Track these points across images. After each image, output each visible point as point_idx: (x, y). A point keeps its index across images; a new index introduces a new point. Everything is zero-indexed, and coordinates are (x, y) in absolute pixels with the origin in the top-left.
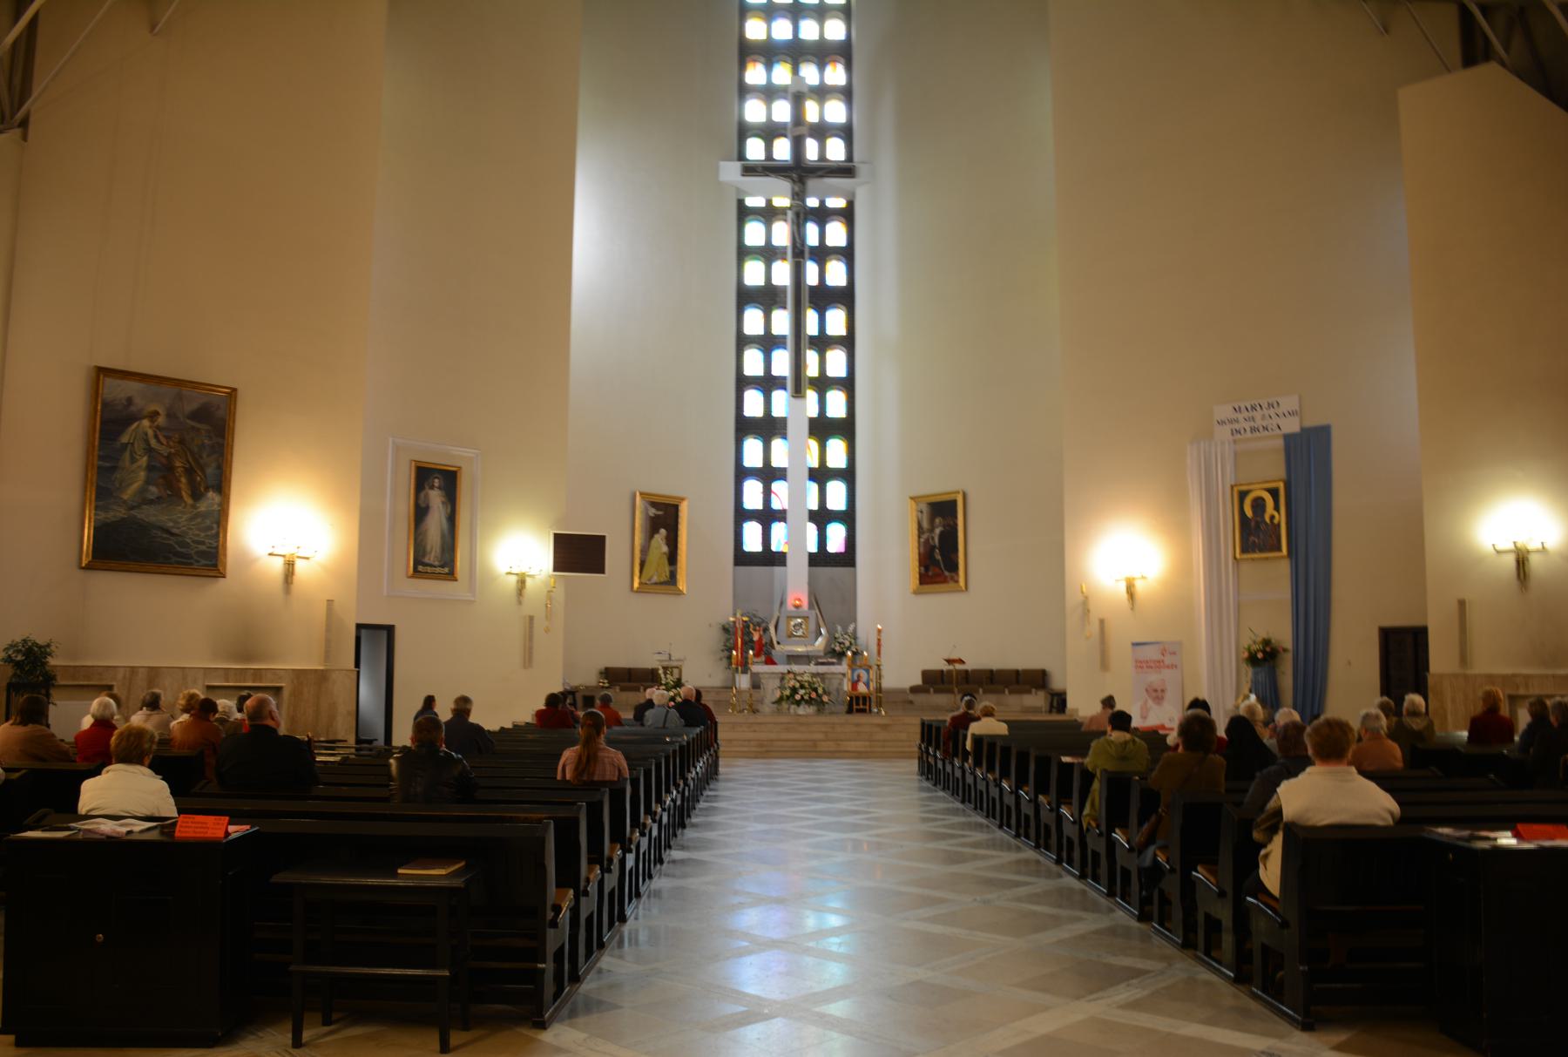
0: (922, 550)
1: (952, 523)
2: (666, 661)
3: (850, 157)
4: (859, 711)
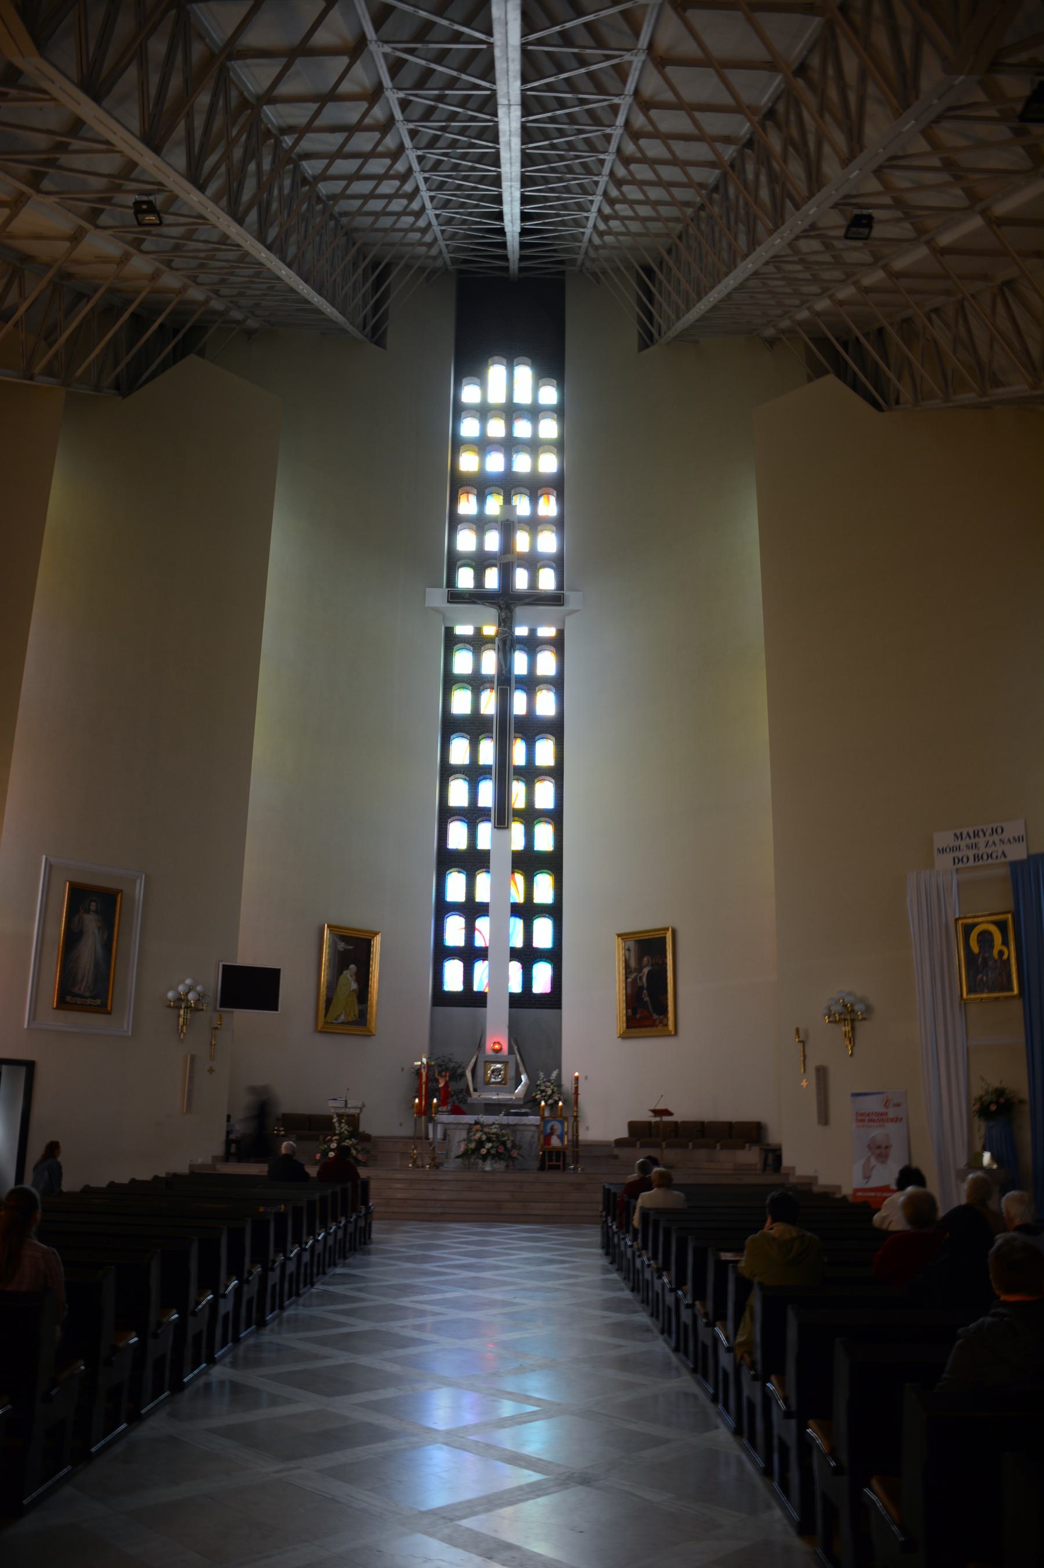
0: (629, 991)
1: (661, 962)
2: (343, 1108)
3: (560, 584)
4: (551, 1168)
